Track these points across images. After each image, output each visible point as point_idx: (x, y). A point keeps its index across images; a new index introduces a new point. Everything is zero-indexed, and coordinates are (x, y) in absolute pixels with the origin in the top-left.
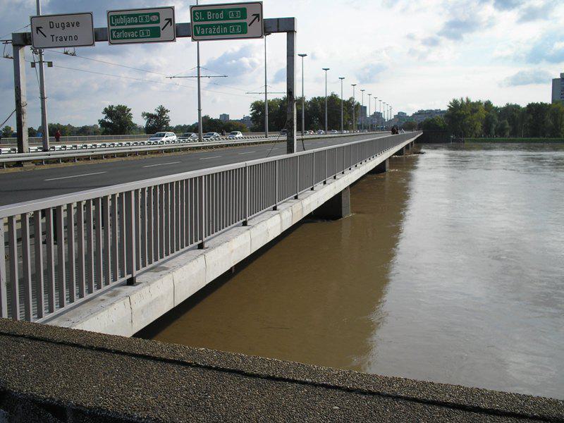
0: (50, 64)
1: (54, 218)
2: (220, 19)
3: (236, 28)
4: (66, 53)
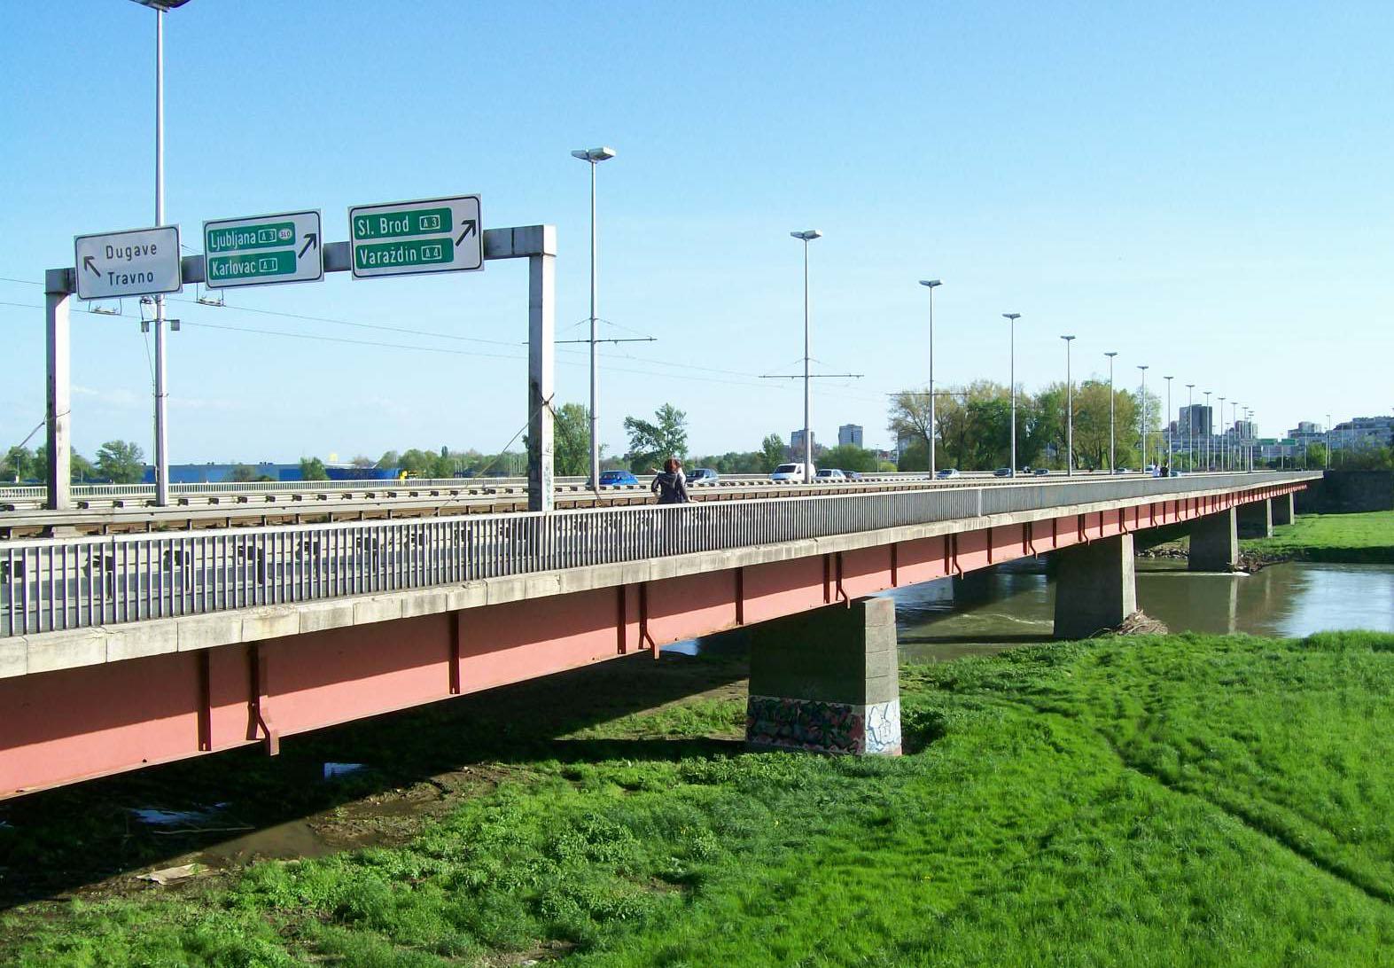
0: (176, 325)
1: (393, 559)
2: (402, 234)
3: (432, 250)
4: (97, 311)
